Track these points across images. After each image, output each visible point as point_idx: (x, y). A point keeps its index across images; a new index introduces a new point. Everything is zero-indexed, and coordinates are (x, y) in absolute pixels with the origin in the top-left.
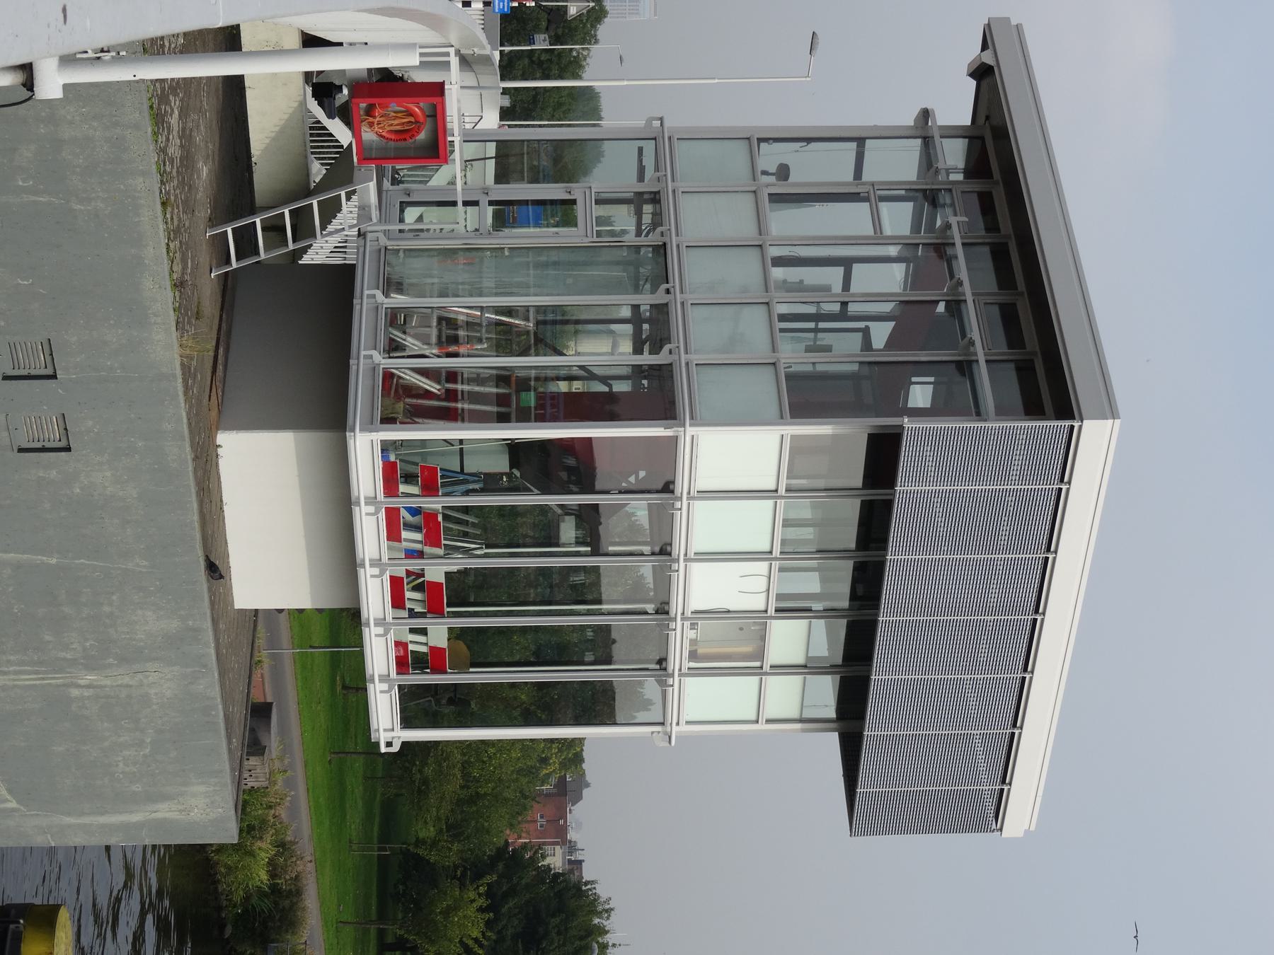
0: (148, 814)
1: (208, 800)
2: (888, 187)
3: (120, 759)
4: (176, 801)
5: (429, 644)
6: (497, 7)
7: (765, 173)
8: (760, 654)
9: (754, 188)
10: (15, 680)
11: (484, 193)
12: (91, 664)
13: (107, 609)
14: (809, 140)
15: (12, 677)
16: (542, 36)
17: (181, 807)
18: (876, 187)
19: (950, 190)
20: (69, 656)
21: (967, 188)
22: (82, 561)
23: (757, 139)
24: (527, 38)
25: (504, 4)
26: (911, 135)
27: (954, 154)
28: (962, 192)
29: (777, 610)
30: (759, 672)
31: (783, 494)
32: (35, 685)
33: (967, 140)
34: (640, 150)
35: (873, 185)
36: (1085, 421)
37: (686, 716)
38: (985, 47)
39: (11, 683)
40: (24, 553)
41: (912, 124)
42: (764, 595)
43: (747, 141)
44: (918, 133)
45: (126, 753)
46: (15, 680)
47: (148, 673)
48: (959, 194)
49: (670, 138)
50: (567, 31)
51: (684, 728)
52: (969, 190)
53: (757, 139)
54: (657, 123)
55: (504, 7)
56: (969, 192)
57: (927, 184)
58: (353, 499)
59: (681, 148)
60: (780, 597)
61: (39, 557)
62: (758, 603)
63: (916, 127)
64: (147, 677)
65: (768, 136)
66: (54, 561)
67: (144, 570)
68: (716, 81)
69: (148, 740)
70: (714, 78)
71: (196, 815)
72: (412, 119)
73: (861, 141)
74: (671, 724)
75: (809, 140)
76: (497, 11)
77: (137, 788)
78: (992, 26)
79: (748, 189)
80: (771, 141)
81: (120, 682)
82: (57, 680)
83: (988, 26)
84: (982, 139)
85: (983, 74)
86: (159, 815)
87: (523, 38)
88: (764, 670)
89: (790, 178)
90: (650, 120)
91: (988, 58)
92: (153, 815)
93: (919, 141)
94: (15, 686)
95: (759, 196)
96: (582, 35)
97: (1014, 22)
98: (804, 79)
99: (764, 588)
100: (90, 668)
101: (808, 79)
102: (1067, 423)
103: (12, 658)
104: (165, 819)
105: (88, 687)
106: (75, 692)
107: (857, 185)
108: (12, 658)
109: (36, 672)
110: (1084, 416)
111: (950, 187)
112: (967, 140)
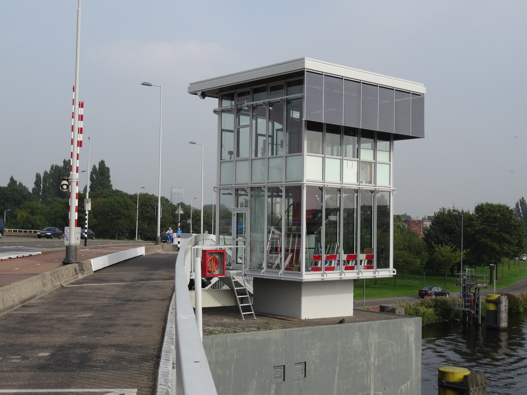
6: (180, 234)
7: (230, 158)
8: (370, 163)
13: (352, 353)
14: (221, 145)
15: (371, 382)
19: (237, 105)
20: (366, 365)
22: (338, 360)
27: (227, 104)
30: (375, 164)
31: (324, 155)
32: (374, 375)
34: (223, 194)
35: (235, 127)
37: (387, 184)
38: (196, 94)
49: (220, 185)
57: (235, 111)
59: (223, 182)
62: (355, 163)
63: (218, 114)
64: (372, 342)
69: (391, 342)
71: (413, 329)
73: (222, 130)
75: (221, 145)
78: (190, 92)
81: (374, 350)
82: (372, 368)
83: (190, 93)
84: (222, 95)
85: (204, 95)
86: (413, 340)
93: (223, 114)
97: (189, 85)
99: (351, 161)
100: (369, 359)
102: (306, 72)
103: (366, 381)
104: (414, 338)
108: (366, 381)
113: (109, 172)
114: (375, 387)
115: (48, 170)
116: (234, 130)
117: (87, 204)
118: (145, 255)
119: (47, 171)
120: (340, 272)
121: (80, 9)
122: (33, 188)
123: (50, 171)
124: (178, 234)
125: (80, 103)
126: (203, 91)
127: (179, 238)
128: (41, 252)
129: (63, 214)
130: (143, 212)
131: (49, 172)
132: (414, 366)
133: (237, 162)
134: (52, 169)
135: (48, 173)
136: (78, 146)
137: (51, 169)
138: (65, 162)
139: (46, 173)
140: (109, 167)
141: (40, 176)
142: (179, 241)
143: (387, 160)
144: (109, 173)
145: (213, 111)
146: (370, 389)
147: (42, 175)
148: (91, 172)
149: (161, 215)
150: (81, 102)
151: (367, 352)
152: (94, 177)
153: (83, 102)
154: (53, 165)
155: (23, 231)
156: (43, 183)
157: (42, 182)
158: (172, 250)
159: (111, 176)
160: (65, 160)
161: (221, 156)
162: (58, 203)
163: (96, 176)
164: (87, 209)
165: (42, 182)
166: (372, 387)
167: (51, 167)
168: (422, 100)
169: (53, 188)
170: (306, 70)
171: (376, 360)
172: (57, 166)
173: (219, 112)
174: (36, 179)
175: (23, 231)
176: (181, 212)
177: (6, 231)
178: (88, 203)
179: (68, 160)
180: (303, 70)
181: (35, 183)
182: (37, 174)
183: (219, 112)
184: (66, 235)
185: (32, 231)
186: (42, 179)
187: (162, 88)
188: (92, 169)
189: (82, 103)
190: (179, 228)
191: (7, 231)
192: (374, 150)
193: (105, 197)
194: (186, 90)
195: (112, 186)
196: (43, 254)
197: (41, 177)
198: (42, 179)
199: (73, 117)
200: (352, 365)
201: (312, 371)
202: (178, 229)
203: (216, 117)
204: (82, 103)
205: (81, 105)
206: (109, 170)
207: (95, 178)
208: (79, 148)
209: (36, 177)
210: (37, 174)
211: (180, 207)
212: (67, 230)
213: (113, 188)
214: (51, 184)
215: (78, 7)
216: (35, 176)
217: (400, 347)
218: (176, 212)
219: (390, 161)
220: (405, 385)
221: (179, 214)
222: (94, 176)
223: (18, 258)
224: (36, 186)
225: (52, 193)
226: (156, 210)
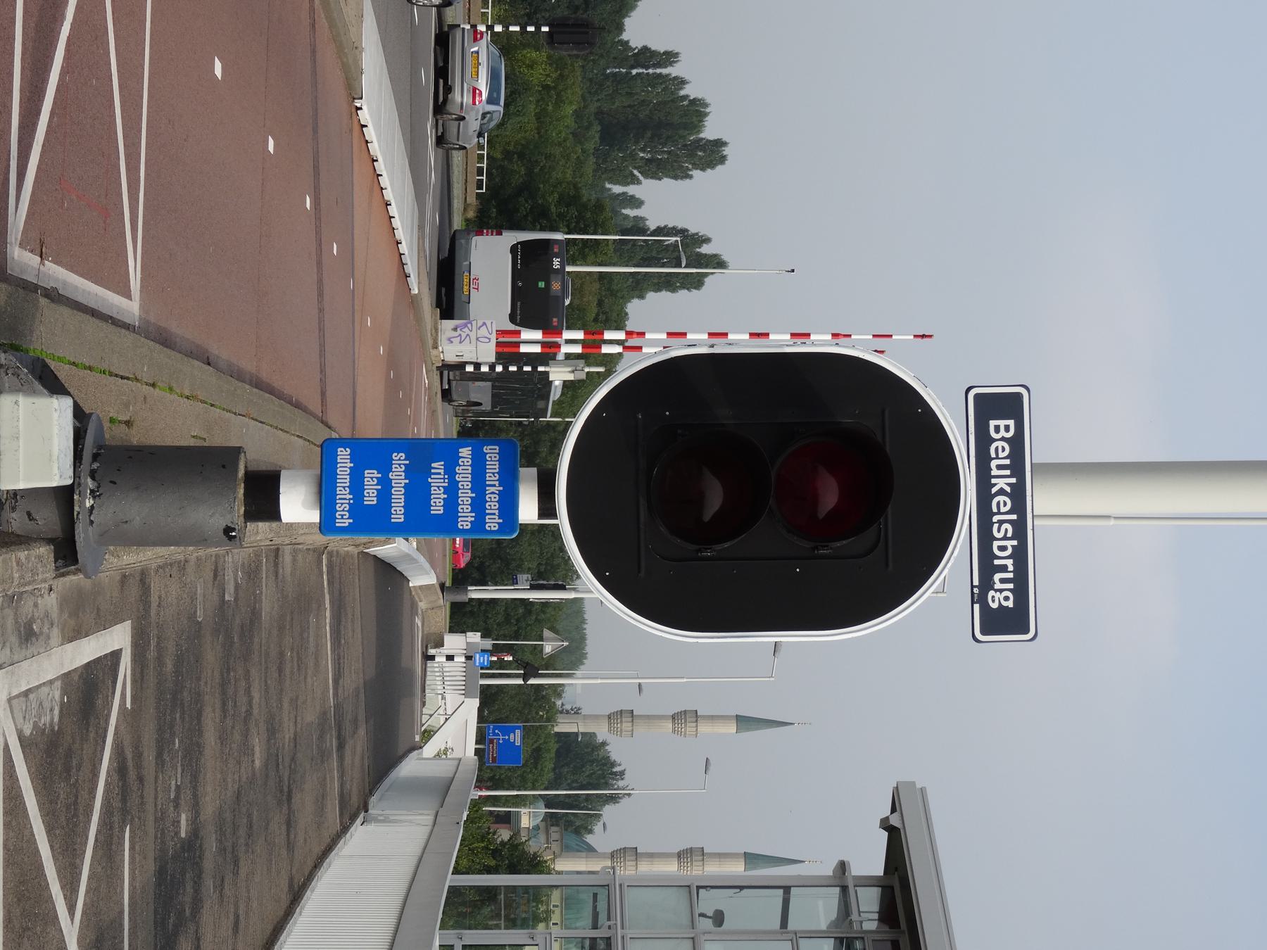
2: (809, 935)
6: (478, 661)
7: (702, 915)
9: (692, 935)
11: (458, 938)
14: (741, 888)
16: (526, 576)
18: (798, 935)
19: (863, 938)
21: (877, 937)
23: (697, 886)
24: (511, 577)
25: (484, 659)
26: (834, 884)
27: (868, 902)
28: (873, 940)
33: (880, 889)
34: (595, 895)
35: (796, 933)
38: (893, 810)
43: (687, 889)
44: (837, 882)
48: (871, 943)
49: (621, 885)
50: (549, 568)
52: (878, 938)
53: (697, 886)
55: (484, 661)
56: (880, 940)
57: (843, 933)
59: (630, 895)
63: (834, 876)
65: (708, 885)
68: (685, 680)
70: (683, 678)
73: (787, 890)
75: (741, 888)
76: (477, 664)
78: (899, 787)
79: (688, 936)
80: (708, 889)
83: (897, 787)
84: (892, 888)
85: (895, 837)
87: (505, 576)
89: (723, 925)
93: (837, 890)
95: (696, 941)
96: (564, 572)
97: (918, 786)
98: (768, 679)
107: (782, 933)
111: (863, 935)
112: (880, 889)
113: (688, 289)
115: (690, 91)
117: (570, 369)
118: (410, 588)
119: (686, 86)
121: (1112, 522)
122: (630, 44)
123: (687, 96)
124: (478, 656)
127: (466, 657)
128: (417, 292)
129: (542, 186)
130: (555, 431)
131: (682, 93)
133: (691, 941)
134: (695, 102)
135: (681, 89)
137: (694, 99)
138: (719, 144)
139: (681, 82)
140: (704, 287)
141: (671, 64)
142: (456, 659)
144: (684, 288)
145: (845, 860)
147: (672, 71)
148: (687, 231)
149: (536, 601)
154: (706, 105)
155: (482, 152)
156: (648, 74)
157: (651, 71)
158: (425, 632)
159: (673, 294)
160: (725, 144)
161: (708, 886)
162: (578, 157)
164: (553, 369)
165: (651, 71)
167: (699, 100)
169: (630, 106)
172: (702, 116)
173: (841, 876)
174: (659, 53)
175: (482, 152)
176: (548, 648)
177: (483, 8)
178: (573, 372)
179: (725, 153)
181: (645, 49)
182: (676, 55)
183: (841, 876)
184: (469, 325)
185: (488, 8)
186: (658, 71)
187: (939, 595)
188: (697, 234)
190: (495, 659)
191: (480, 178)
193: (600, 303)
194: (905, 778)
195: (642, 297)
196: (411, 297)
197: (666, 67)
198: (658, 71)
199: (835, 335)
202: (492, 655)
203: (828, 870)
206: (695, 288)
209: (666, 53)
210: (677, 54)
211: (566, 644)
212: (485, 326)
213: (636, 302)
214: (643, 101)
215: (1115, 518)
216: (670, 50)
218: (547, 633)
221: (543, 641)
223: (397, 255)
224: (636, 51)
225: (614, 103)
226: (553, 583)
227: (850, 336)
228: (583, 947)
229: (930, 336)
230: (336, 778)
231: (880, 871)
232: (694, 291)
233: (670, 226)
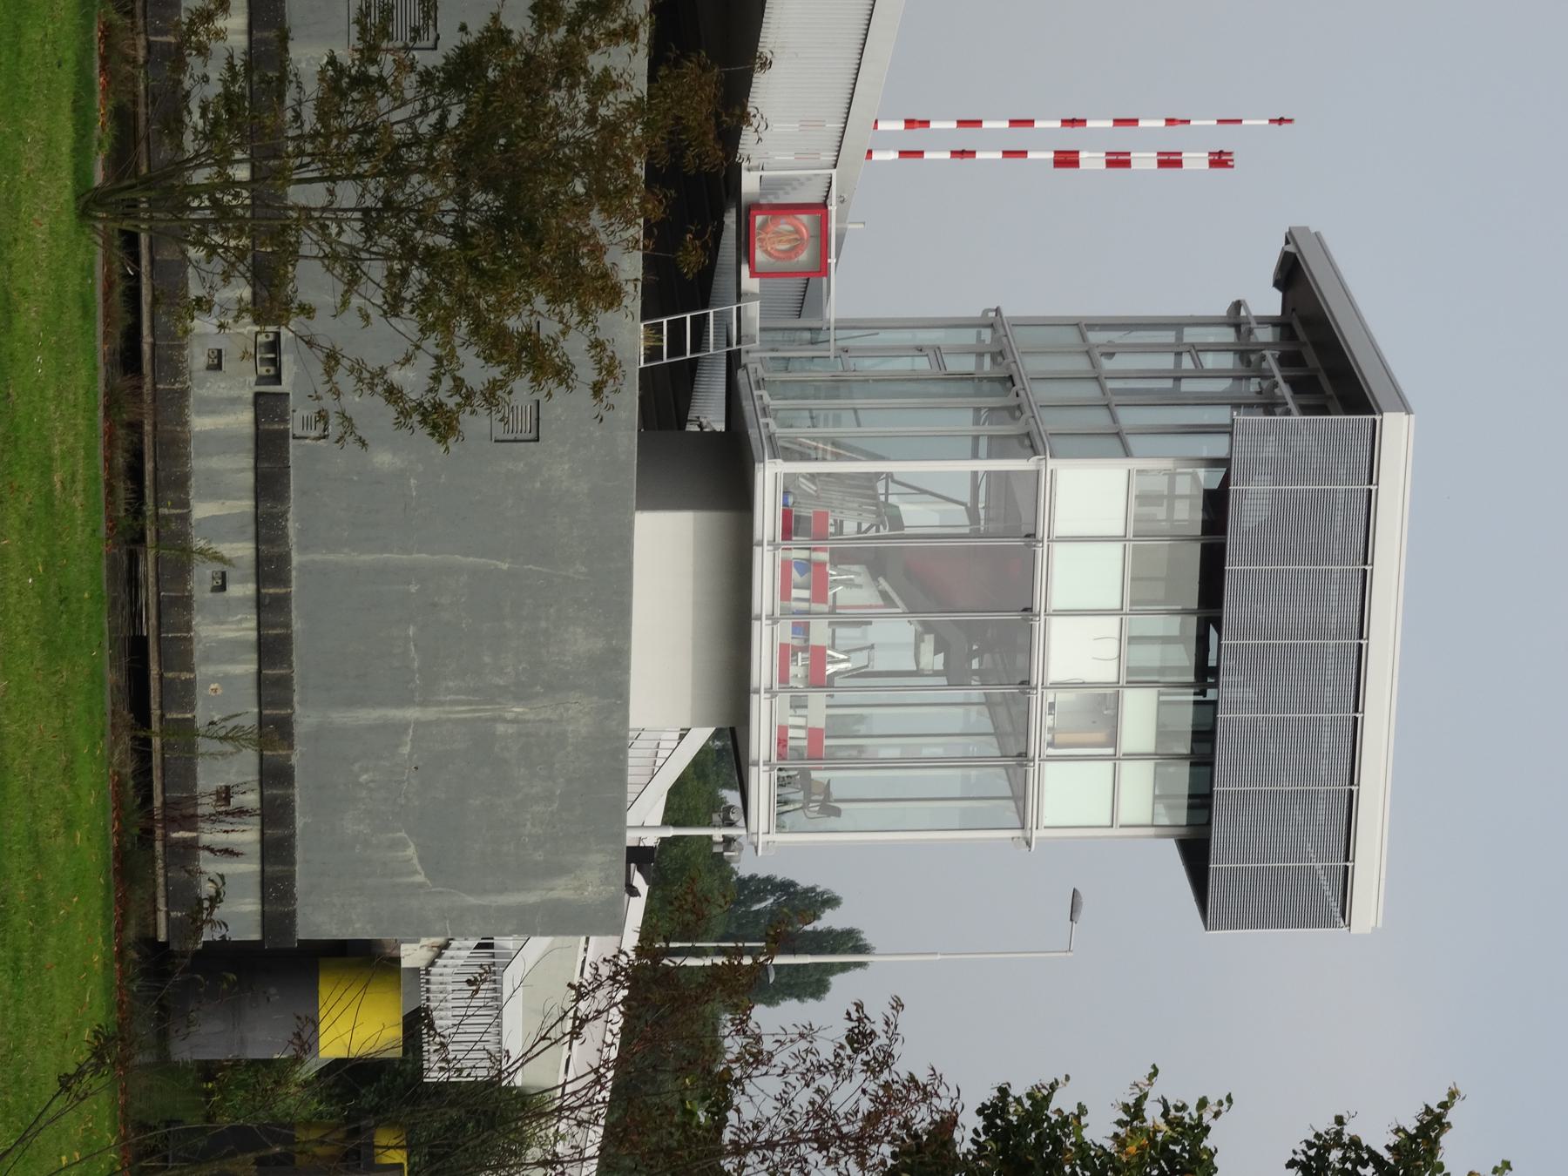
0: (544, 892)
1: (602, 874)
3: (529, 816)
4: (573, 875)
5: (809, 726)
8: (1113, 741)
9: (1086, 349)
10: (450, 712)
12: (521, 693)
13: (543, 624)
15: (447, 708)
17: (576, 883)
20: (501, 683)
22: (530, 566)
29: (1127, 682)
31: (1131, 538)
32: (465, 719)
36: (1385, 414)
38: (1287, 242)
39: (444, 716)
40: (481, 557)
41: (1225, 314)
42: (1116, 661)
45: (536, 808)
46: (450, 712)
47: (569, 705)
51: (1042, 833)
54: (992, 314)
58: (755, 541)
60: (1130, 671)
61: (494, 562)
62: (1108, 673)
64: (567, 710)
66: (505, 566)
67: (582, 578)
68: (939, 957)
69: (558, 792)
70: (936, 953)
72: (797, 236)
74: (1031, 829)
77: (539, 856)
81: (542, 716)
82: (486, 712)
83: (1290, 232)
86: (555, 894)
88: (1121, 684)
90: (986, 312)
91: (1291, 248)
92: (551, 893)
94: (449, 720)
97: (1313, 231)
99: (1116, 654)
100: (519, 698)
101: (1069, 954)
102: (1371, 417)
103: (451, 684)
104: (559, 900)
105: (514, 721)
106: (501, 728)
108: (451, 684)
109: (469, 703)
110: (1382, 407)
114: (429, 724)
116: (1185, 344)
120: (777, 613)
125: (1230, 154)
126: (1298, 255)
132: (472, 900)
136: (1056, 152)
140: (828, 996)
143: (1125, 816)
146: (424, 704)
150: (1232, 160)
151: (539, 688)
152: (760, 901)
153: (1232, 166)
163: (771, 912)
166: (431, 713)
168: (1331, 923)
170: (1378, 418)
171: (511, 729)
173: (1236, 318)
180: (1375, 409)
183: (1236, 318)
188: (813, 889)
189: (1230, 163)
192: (1156, 754)
194: (1297, 222)
200: (508, 625)
201: (510, 466)
203: (1222, 310)
204: (1230, 163)
205: (1220, 160)
207: (756, 907)
208: (1052, 155)
217: (541, 832)
219: (1121, 826)
220: (415, 861)
222: (771, 901)
227: (1188, 121)
228: (839, 1173)
229: (1290, 121)
230: (540, 569)
231: (1278, 312)
232: (811, 1002)
233: (762, 874)
